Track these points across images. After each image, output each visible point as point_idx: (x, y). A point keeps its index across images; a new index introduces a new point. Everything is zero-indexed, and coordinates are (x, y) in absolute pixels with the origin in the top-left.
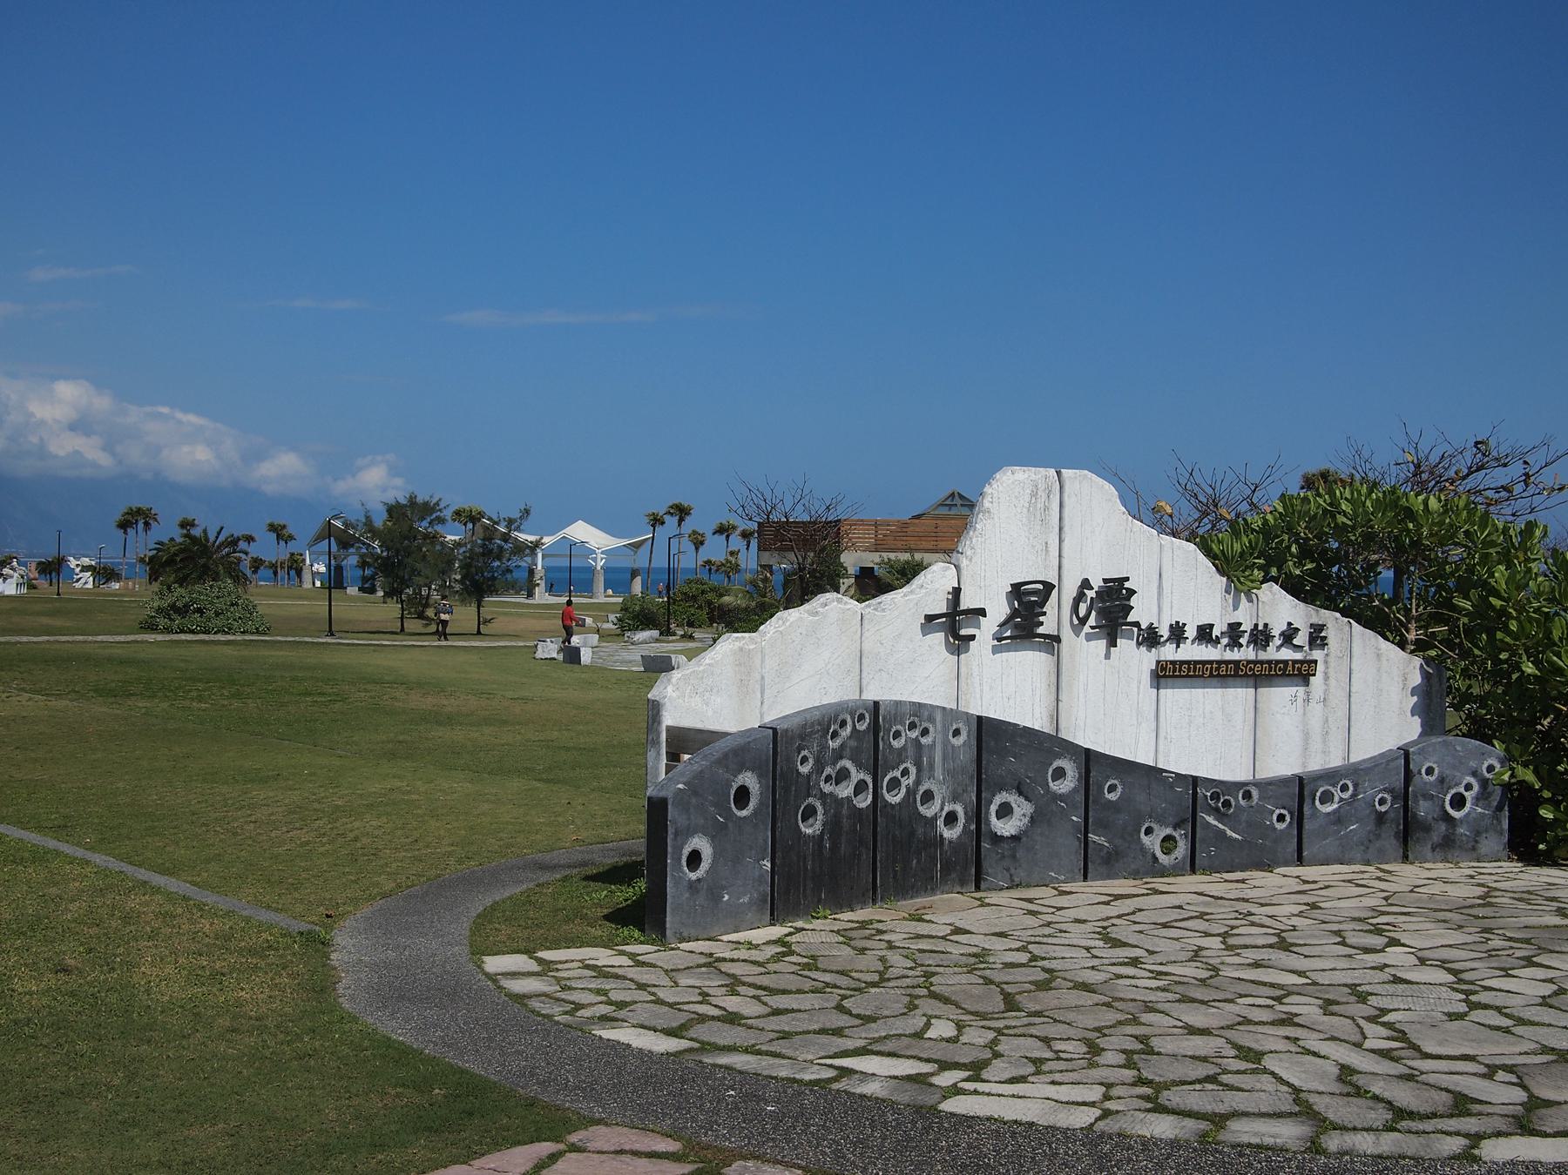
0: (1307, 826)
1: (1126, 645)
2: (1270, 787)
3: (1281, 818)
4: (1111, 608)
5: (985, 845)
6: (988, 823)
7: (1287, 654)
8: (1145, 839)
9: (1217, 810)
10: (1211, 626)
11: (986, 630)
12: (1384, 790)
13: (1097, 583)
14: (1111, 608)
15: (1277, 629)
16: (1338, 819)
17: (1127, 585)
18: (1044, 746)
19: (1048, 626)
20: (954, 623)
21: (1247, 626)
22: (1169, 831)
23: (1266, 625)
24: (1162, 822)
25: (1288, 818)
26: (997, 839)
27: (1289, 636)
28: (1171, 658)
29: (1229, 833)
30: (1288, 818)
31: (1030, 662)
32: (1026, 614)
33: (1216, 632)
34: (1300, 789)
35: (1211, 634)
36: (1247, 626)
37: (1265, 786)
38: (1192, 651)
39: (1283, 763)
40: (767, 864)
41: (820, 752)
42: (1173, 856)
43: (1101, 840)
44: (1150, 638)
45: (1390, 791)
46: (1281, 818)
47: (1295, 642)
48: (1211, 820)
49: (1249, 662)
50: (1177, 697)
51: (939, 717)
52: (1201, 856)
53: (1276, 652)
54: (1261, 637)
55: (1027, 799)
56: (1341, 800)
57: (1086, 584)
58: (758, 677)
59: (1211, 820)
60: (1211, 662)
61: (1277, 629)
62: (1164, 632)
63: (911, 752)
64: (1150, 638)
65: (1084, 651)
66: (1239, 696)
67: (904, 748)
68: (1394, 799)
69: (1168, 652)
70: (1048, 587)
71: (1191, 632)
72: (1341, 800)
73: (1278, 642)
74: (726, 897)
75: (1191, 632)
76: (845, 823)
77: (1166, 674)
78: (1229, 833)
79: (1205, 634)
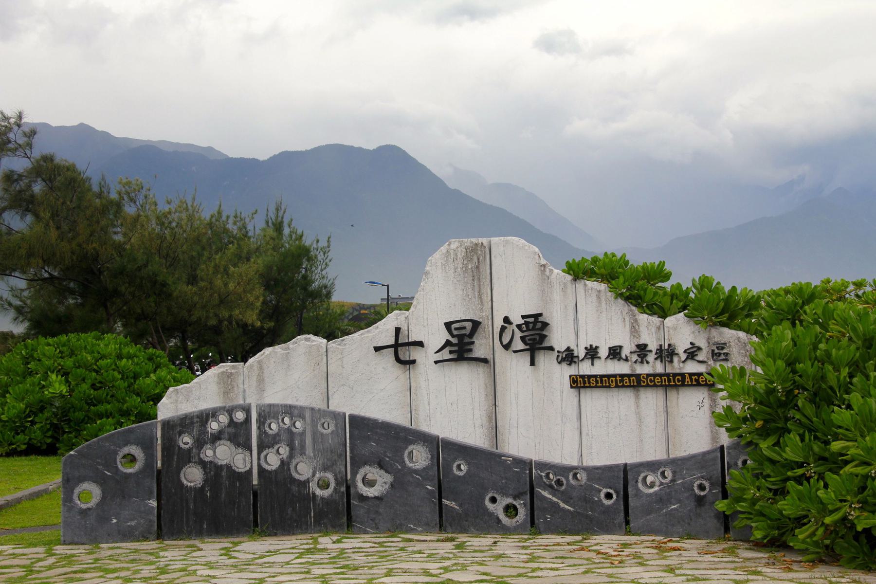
0: (632, 503)
1: (546, 361)
2: (599, 474)
3: (609, 496)
4: (534, 335)
5: (354, 502)
6: (356, 487)
7: (692, 367)
8: (490, 506)
9: (551, 486)
10: (621, 347)
11: (425, 358)
12: (702, 477)
13: (517, 320)
14: (534, 335)
15: (682, 346)
16: (662, 499)
17: (540, 319)
18: (398, 437)
19: (480, 349)
20: (402, 350)
21: (653, 346)
22: (510, 500)
23: (670, 345)
24: (505, 494)
25: (615, 496)
26: (363, 498)
27: (692, 353)
28: (588, 372)
29: (562, 505)
30: (615, 496)
31: (465, 379)
32: (461, 345)
33: (625, 352)
34: (624, 477)
35: (620, 353)
36: (653, 346)
37: (593, 472)
38: (604, 367)
39: (602, 455)
40: (154, 503)
41: (200, 435)
42: (515, 520)
43: (453, 504)
44: (569, 357)
45: (709, 479)
46: (609, 496)
47: (697, 358)
48: (546, 494)
49: (648, 375)
50: (596, 401)
51: (308, 415)
52: (539, 521)
53: (678, 366)
54: (666, 354)
55: (387, 471)
56: (661, 484)
57: (507, 320)
58: (241, 390)
59: (546, 494)
60: (615, 376)
61: (682, 346)
62: (582, 354)
63: (284, 436)
64: (569, 357)
65: (514, 367)
66: (651, 399)
67: (278, 434)
68: (712, 485)
69: (586, 368)
70: (476, 324)
71: (603, 352)
72: (661, 484)
73: (683, 357)
74: (114, 521)
75: (603, 352)
76: (226, 482)
77: (579, 383)
78: (562, 505)
79: (615, 353)
